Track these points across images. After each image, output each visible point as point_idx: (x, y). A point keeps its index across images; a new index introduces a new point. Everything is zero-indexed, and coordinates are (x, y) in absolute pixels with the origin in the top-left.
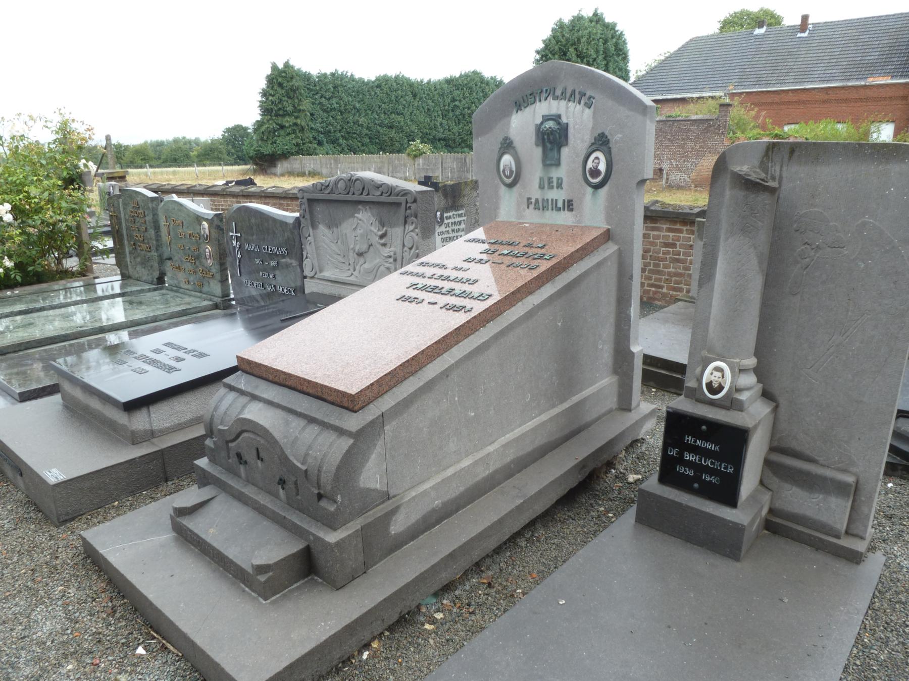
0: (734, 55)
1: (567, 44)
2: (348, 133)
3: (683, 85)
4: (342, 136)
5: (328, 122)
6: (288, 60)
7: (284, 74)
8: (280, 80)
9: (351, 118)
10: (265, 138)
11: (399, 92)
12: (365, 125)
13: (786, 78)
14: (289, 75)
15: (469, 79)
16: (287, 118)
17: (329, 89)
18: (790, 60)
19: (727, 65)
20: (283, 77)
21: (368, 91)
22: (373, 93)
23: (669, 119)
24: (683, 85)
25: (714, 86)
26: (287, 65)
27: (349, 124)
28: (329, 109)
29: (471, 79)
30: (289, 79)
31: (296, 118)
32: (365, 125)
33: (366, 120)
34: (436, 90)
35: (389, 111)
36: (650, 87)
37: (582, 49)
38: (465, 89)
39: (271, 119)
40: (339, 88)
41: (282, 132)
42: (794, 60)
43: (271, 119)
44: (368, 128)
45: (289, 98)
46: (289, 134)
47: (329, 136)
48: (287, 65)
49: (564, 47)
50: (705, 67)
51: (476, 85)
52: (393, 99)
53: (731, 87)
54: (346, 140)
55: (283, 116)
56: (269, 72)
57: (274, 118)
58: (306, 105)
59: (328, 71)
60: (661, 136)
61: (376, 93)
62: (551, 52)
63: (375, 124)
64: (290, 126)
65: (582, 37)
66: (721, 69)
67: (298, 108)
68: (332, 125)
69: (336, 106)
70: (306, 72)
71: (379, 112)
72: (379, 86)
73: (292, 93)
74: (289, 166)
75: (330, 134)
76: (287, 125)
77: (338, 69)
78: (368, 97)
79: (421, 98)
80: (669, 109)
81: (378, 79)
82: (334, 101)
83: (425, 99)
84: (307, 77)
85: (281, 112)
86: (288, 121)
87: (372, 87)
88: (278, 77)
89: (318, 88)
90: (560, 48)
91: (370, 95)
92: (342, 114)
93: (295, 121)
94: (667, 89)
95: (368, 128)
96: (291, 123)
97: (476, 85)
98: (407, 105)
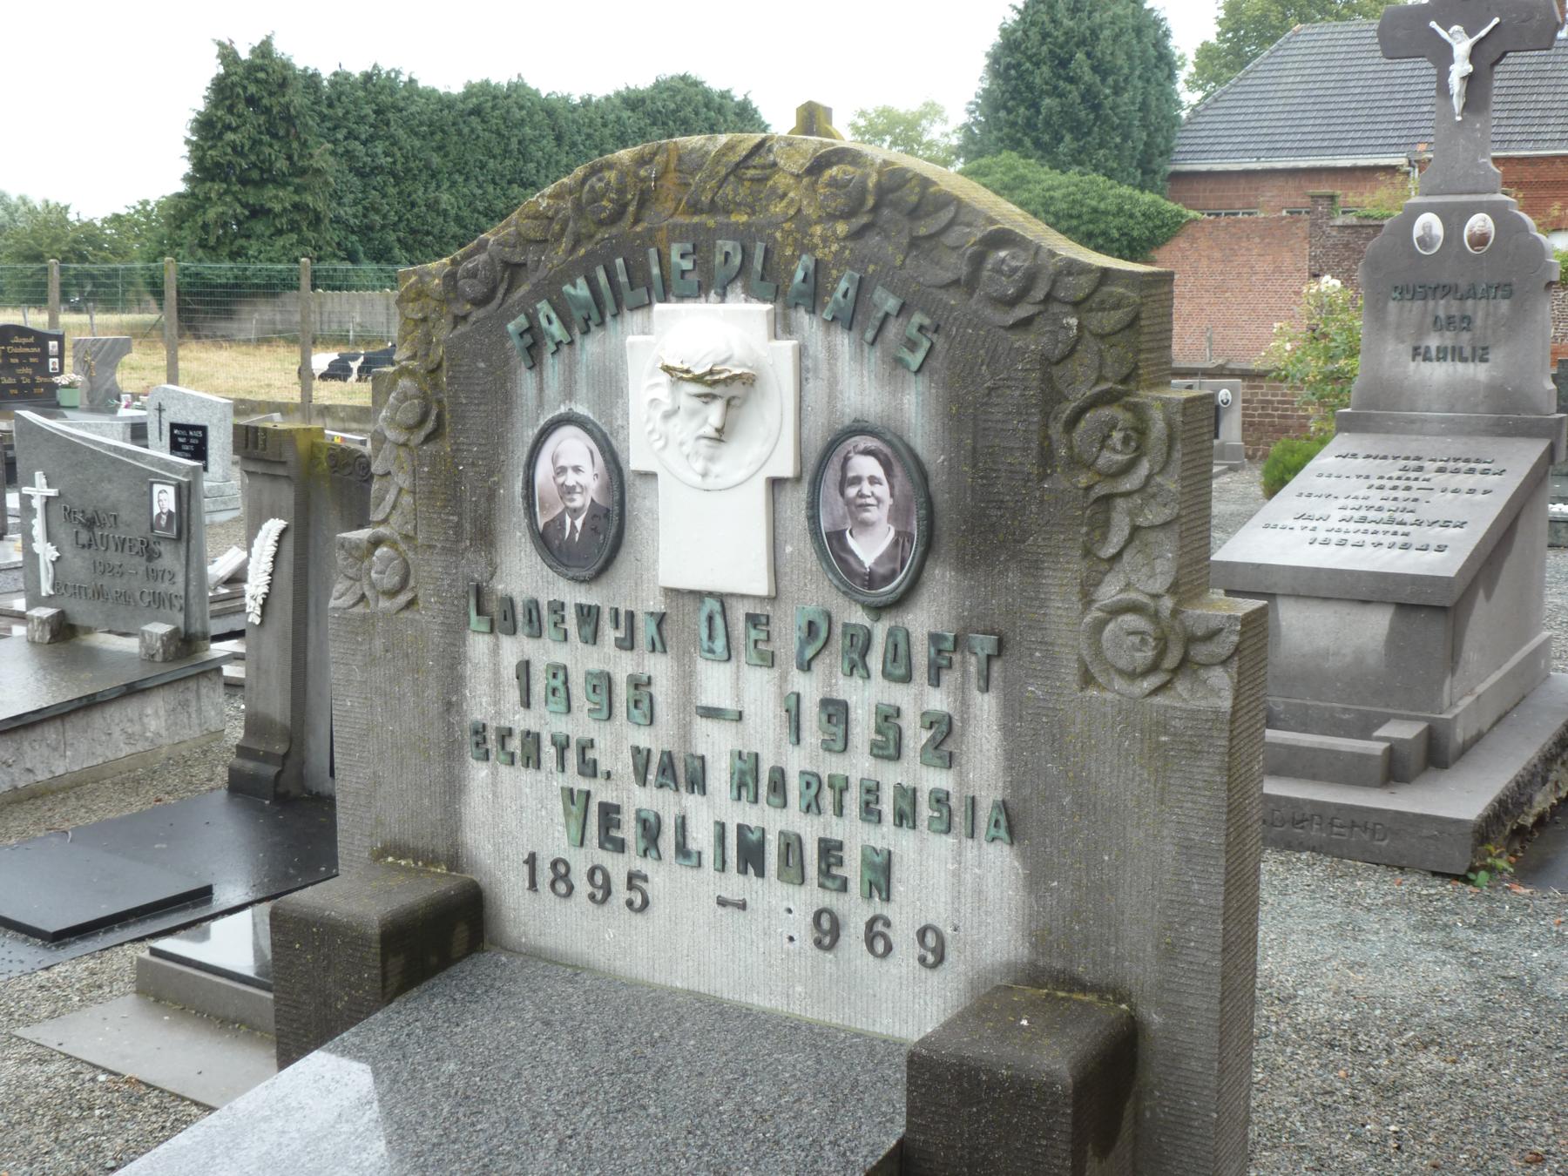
0: (1409, 73)
1: (1067, 42)
2: (413, 232)
3: (1304, 137)
4: (399, 240)
5: (366, 203)
6: (269, 37)
7: (261, 75)
8: (252, 89)
9: (420, 193)
10: (212, 241)
11: (527, 130)
12: (453, 212)
13: (1543, 129)
14: (276, 77)
15: (679, 98)
16: (270, 191)
17: (366, 116)
18: (1543, 90)
19: (1398, 96)
20: (257, 81)
21: (454, 124)
22: (466, 130)
23: (1365, 222)
24: (1304, 137)
25: (1380, 141)
26: (264, 50)
27: (416, 210)
28: (367, 169)
29: (684, 99)
30: (275, 88)
31: (298, 190)
32: (453, 212)
33: (453, 200)
34: (605, 125)
35: (503, 176)
36: (1224, 140)
37: (1103, 53)
38: (671, 123)
39: (226, 192)
40: (390, 115)
41: (259, 227)
42: (1552, 90)
43: (226, 192)
44: (459, 220)
45: (275, 136)
46: (280, 232)
47: (370, 240)
48: (264, 50)
49: (1061, 47)
50: (1348, 99)
51: (697, 114)
52: (514, 145)
53: (1421, 147)
54: (407, 250)
55: (260, 184)
56: (216, 68)
57: (236, 188)
58: (322, 156)
59: (357, 68)
60: (1348, 258)
61: (472, 131)
62: (1029, 58)
63: (475, 210)
64: (285, 210)
65: (1101, 27)
66: (1385, 104)
67: (300, 164)
68: (377, 211)
69: (385, 161)
70: (306, 69)
71: (481, 178)
72: (477, 111)
73: (282, 124)
74: (278, 317)
75: (372, 235)
76: (278, 208)
77: (380, 64)
78: (455, 138)
79: (573, 145)
80: (1275, 192)
81: (471, 91)
82: (379, 148)
83: (582, 147)
84: (311, 81)
85: (255, 175)
86: (278, 198)
87: (462, 114)
88: (246, 82)
89: (340, 112)
90: (1050, 51)
91: (460, 133)
92: (398, 181)
93: (297, 198)
94: (1266, 146)
95: (459, 220)
96: (287, 205)
97: (697, 114)
98: (544, 163)
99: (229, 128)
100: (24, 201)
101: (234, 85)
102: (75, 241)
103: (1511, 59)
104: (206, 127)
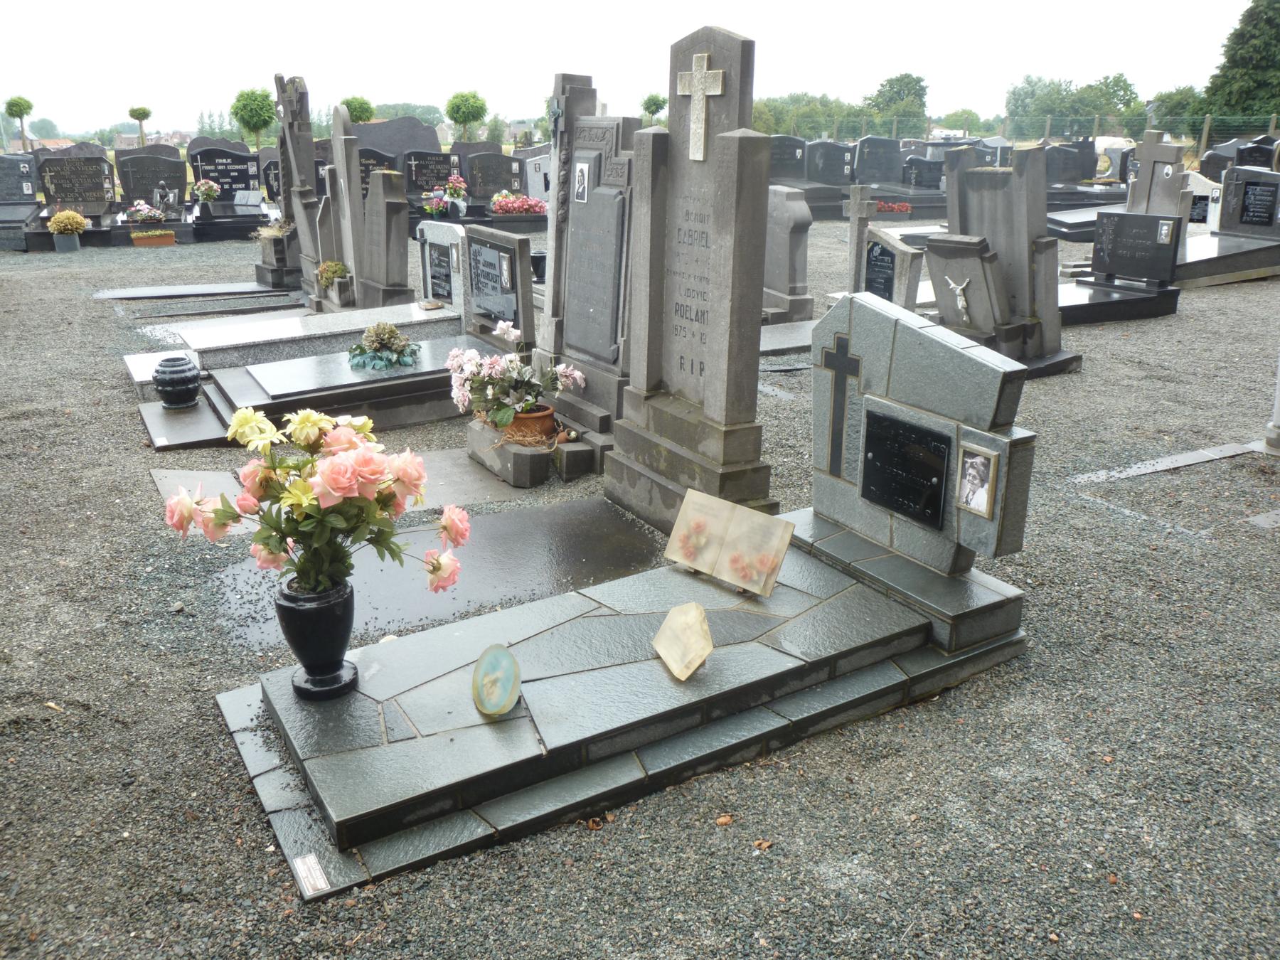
41: (1262, 93)
43: (1245, 74)
55: (1266, 69)
99: (1253, 37)
100: (1040, 80)
101: (1260, 12)
102: (1073, 101)
103: (754, 645)
104: (1239, 38)
